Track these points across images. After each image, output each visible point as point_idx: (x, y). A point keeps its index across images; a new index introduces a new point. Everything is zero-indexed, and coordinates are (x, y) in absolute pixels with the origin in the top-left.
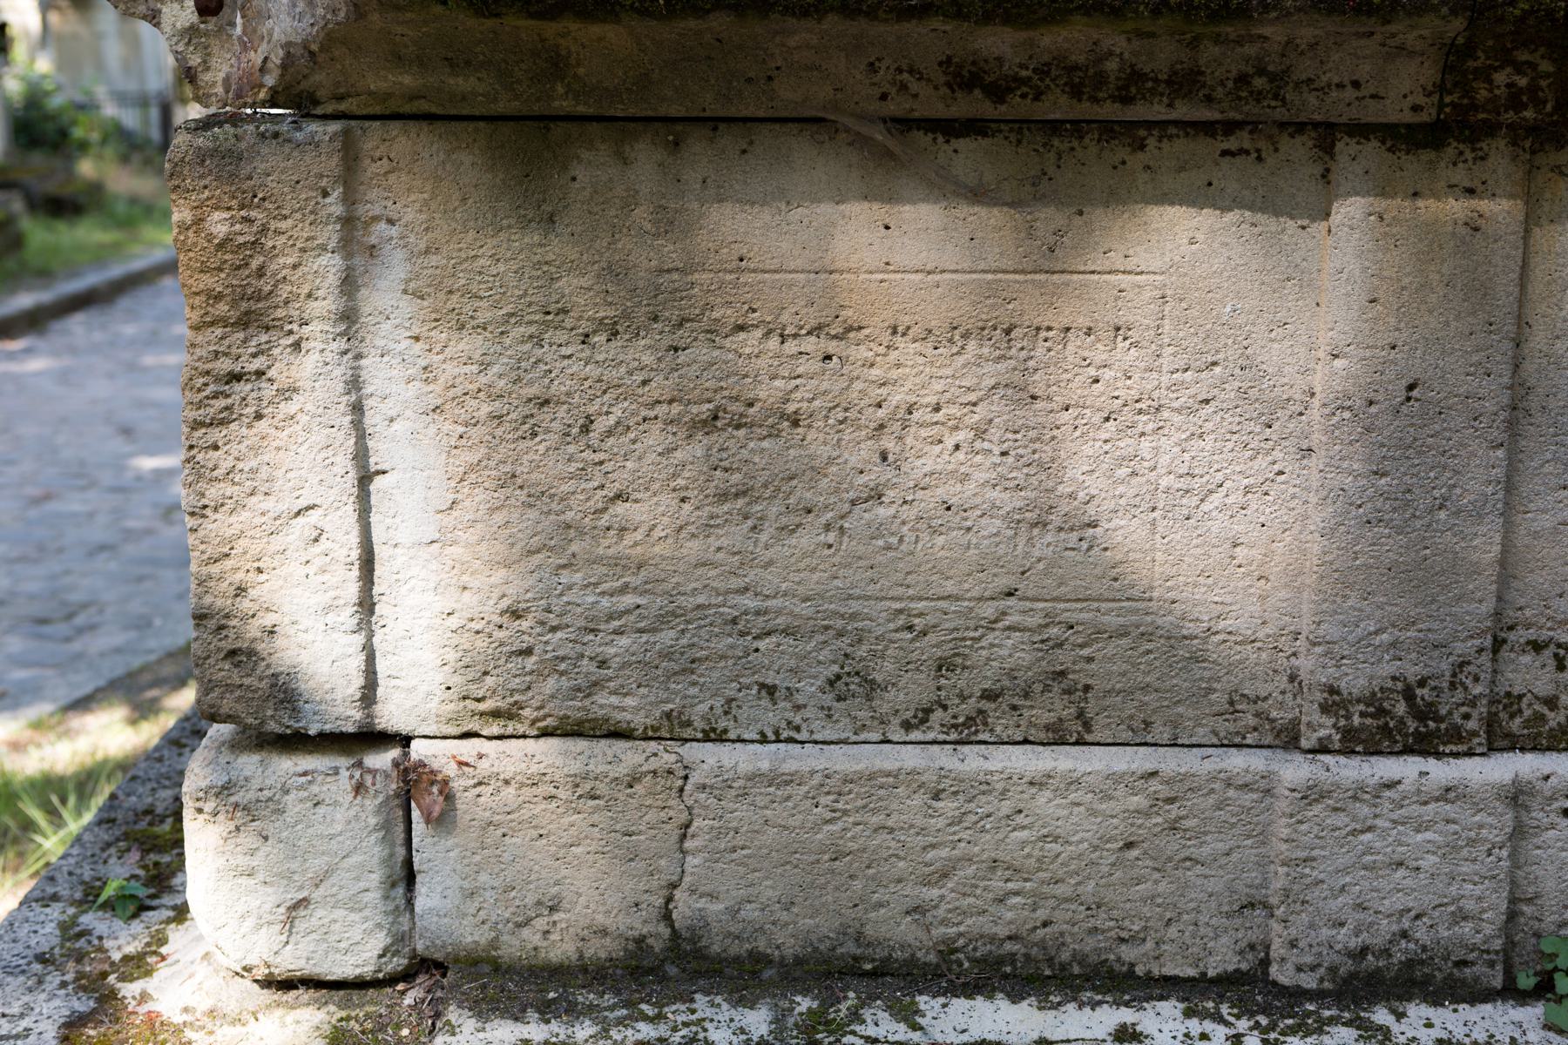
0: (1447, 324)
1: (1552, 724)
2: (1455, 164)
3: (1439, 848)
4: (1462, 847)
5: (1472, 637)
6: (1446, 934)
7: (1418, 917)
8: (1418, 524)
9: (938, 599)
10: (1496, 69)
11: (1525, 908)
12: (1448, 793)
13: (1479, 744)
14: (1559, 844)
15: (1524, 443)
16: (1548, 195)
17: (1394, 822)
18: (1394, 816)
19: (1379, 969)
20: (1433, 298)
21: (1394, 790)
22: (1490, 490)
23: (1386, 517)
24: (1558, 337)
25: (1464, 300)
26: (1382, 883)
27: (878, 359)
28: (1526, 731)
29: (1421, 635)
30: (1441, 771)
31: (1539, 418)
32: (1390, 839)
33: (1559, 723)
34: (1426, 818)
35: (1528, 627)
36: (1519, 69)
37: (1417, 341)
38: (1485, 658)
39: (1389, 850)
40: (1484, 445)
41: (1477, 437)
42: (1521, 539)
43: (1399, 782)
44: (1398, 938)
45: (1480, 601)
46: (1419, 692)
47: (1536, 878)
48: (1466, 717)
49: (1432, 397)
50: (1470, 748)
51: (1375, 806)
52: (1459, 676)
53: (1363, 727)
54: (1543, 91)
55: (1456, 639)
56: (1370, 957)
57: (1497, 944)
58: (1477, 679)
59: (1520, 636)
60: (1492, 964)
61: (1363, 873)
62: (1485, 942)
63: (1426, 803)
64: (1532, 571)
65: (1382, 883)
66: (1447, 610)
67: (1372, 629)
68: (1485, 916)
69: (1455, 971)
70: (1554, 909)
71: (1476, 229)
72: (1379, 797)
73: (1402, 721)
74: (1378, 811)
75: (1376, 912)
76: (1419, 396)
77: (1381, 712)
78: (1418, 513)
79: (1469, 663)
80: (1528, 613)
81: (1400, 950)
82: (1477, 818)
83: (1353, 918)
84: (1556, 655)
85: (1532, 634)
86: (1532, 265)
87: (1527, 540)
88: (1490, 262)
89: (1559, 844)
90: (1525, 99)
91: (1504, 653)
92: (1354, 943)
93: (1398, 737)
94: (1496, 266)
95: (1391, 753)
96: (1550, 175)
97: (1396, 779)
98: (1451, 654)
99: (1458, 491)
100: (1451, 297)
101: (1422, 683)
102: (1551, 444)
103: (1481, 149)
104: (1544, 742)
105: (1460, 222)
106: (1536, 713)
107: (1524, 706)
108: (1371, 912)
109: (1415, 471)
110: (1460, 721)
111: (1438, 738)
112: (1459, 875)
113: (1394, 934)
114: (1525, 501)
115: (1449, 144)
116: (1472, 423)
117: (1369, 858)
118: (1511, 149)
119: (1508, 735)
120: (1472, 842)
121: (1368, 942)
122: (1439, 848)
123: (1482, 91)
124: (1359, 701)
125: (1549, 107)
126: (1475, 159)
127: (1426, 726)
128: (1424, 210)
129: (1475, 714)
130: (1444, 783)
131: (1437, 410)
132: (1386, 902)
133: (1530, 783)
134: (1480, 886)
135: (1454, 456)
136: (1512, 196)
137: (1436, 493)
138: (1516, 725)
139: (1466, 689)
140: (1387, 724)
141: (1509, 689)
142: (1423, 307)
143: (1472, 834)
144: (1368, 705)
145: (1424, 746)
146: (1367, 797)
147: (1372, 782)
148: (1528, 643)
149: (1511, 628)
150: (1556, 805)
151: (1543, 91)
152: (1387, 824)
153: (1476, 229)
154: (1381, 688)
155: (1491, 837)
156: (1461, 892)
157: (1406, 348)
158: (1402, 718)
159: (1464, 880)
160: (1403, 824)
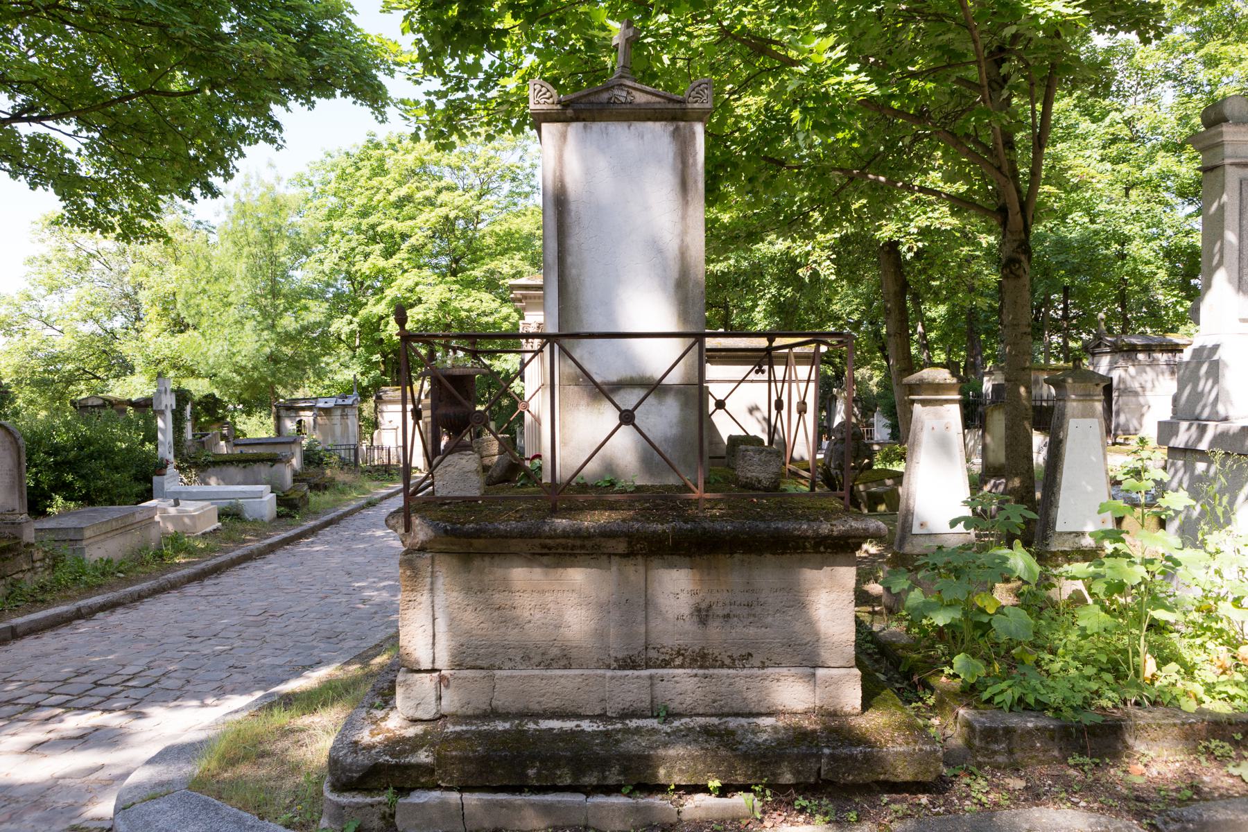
12: (638, 677)
30: (636, 673)
145: (634, 668)
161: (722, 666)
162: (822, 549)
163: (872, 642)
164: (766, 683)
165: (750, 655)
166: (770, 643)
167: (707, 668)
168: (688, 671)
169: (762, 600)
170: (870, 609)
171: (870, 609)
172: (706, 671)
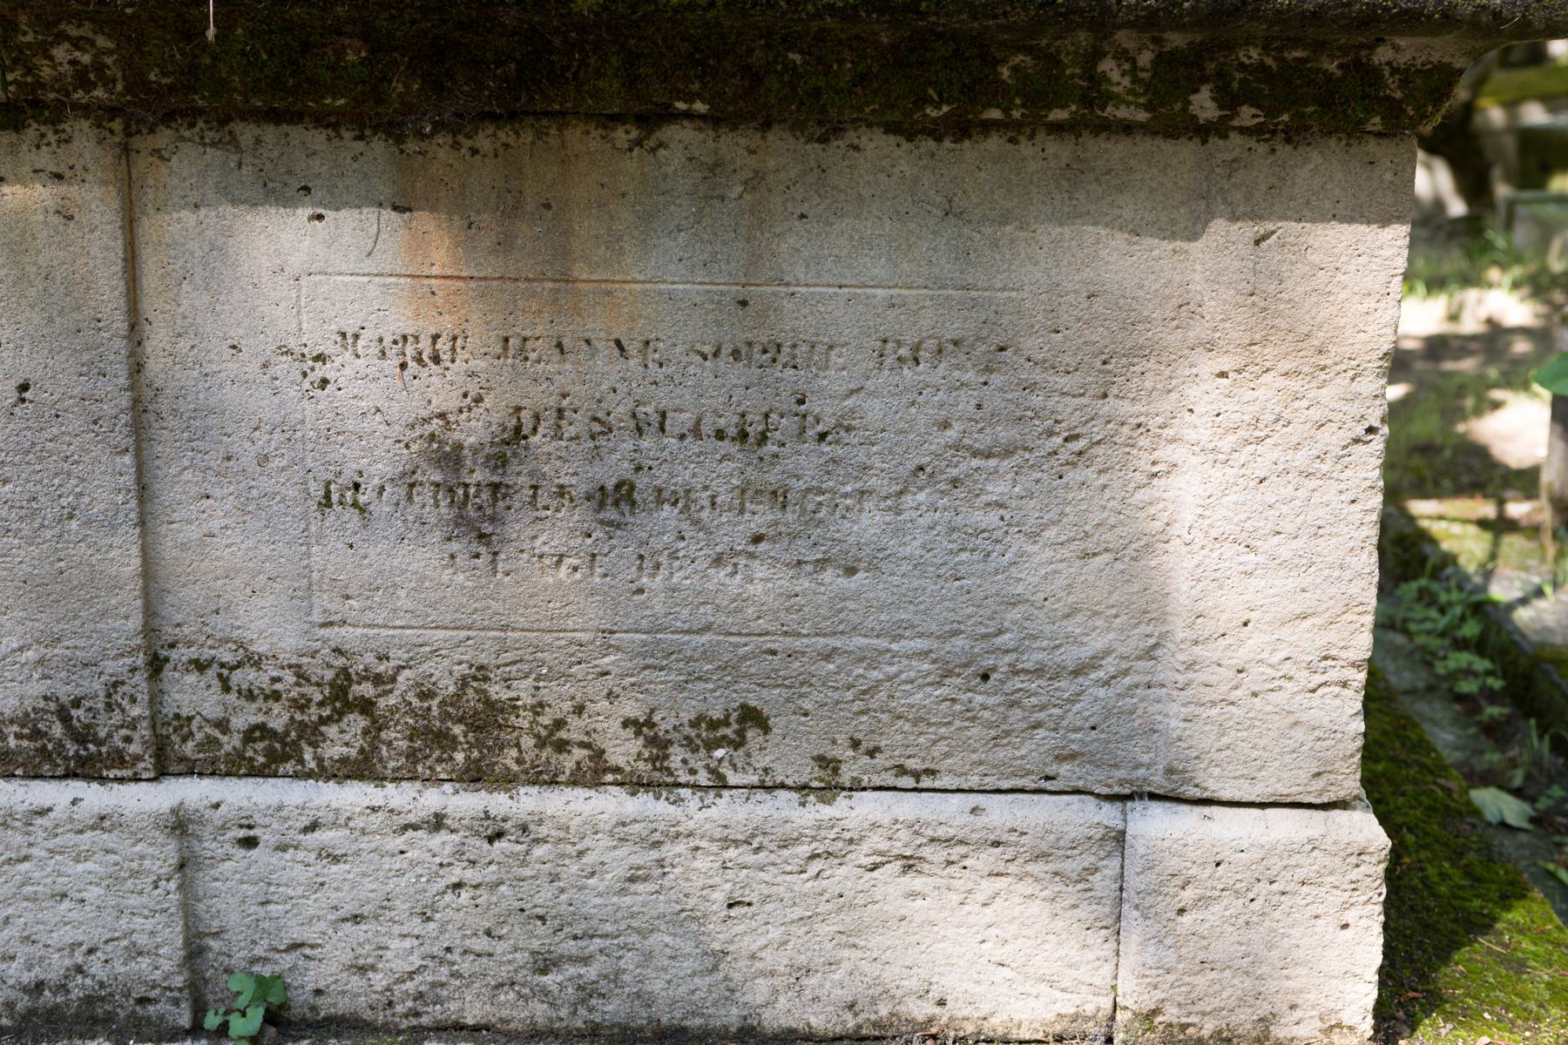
0: (51, 320)
1: (228, 748)
2: (38, 147)
3: (101, 879)
4: (125, 879)
5: (122, 655)
6: (123, 969)
7: (91, 951)
8: (48, 534)
9: (437, 627)
10: (52, 44)
11: (212, 943)
12: (101, 822)
13: (145, 769)
14: (238, 876)
15: (160, 448)
16: (151, 182)
17: (51, 851)
18: (51, 844)
19: (57, 1006)
20: (32, 292)
21: (46, 818)
22: (120, 499)
23: (14, 526)
24: (179, 335)
25: (67, 295)
26: (45, 916)
27: (1172, 315)
28: (201, 755)
29: (68, 652)
30: (95, 797)
31: (171, 422)
32: (49, 870)
33: (234, 748)
34: (83, 848)
35: (190, 644)
36: (77, 43)
37: (22, 338)
38: (140, 678)
39: (49, 880)
40: (108, 451)
41: (99, 442)
42: (168, 550)
43: (50, 810)
44: (73, 973)
45: (127, 618)
46: (74, 712)
47: (218, 912)
48: (128, 740)
49: (46, 399)
50: (136, 774)
51: (28, 833)
52: (114, 697)
53: (19, 751)
54: (109, 69)
55: (105, 657)
56: (47, 993)
57: (178, 981)
58: (133, 700)
59: (181, 654)
60: (176, 1002)
61: (25, 904)
62: (165, 979)
63: (81, 832)
64: (184, 586)
65: (45, 916)
66: (92, 626)
67: (15, 645)
68: (161, 952)
69: (138, 1008)
70: (242, 944)
71: (71, 218)
72: (31, 825)
73: (60, 744)
74: (32, 839)
75: (45, 946)
76: (31, 398)
77: (36, 734)
78: (46, 523)
79: (123, 683)
80: (186, 630)
81: (77, 986)
82: (137, 848)
83: (23, 951)
84: (220, 676)
85: (192, 653)
86: (144, 257)
87: (175, 553)
88: (88, 253)
89: (238, 876)
90: (92, 76)
91: (167, 673)
92: (27, 978)
93: (58, 761)
94: (95, 258)
95: (53, 777)
96: (151, 159)
97: (46, 807)
98: (101, 673)
99: (86, 500)
100: (52, 291)
101: (76, 703)
102: (186, 449)
103: (64, 131)
104: (222, 767)
105: (51, 210)
106: (208, 736)
107: (194, 728)
108: (41, 945)
109: (38, 477)
110: (121, 745)
111: (101, 762)
112: (127, 908)
113: (68, 969)
114: (168, 510)
115: (30, 125)
116: (91, 427)
117: (28, 889)
118: (96, 131)
119: (183, 759)
120: (135, 874)
121: (42, 977)
122: (101, 879)
123: (45, 68)
124: (12, 722)
125: (119, 87)
126: (59, 142)
127: (86, 749)
128: (11, 197)
129: (136, 736)
130: (96, 810)
131: (53, 412)
132: (54, 935)
133: (197, 811)
134: (150, 920)
135: (77, 462)
136: (104, 183)
137: (64, 502)
138: (189, 748)
139: (123, 711)
140: (44, 747)
141: (177, 711)
142: (23, 301)
143: (135, 865)
144: (23, 726)
145: (86, 769)
146: (17, 824)
147: (21, 808)
148: (190, 662)
149: (172, 646)
150: (230, 835)
151: (109, 69)
152: (44, 854)
153: (71, 218)
154: (34, 709)
155: (155, 868)
156: (132, 926)
157: (11, 345)
158: (61, 740)
159: (133, 914)
160: (61, 853)
161: (595, 773)
162: (1204, 105)
163: (1479, 646)
164: (842, 877)
165: (752, 717)
166: (871, 659)
167: (508, 781)
168: (399, 796)
169: (825, 409)
170: (1488, 510)
171: (1488, 510)
172: (498, 802)
